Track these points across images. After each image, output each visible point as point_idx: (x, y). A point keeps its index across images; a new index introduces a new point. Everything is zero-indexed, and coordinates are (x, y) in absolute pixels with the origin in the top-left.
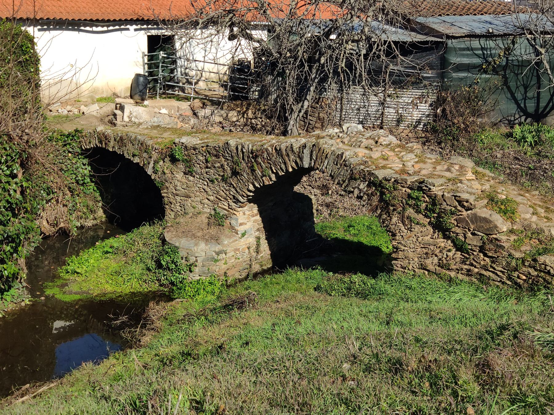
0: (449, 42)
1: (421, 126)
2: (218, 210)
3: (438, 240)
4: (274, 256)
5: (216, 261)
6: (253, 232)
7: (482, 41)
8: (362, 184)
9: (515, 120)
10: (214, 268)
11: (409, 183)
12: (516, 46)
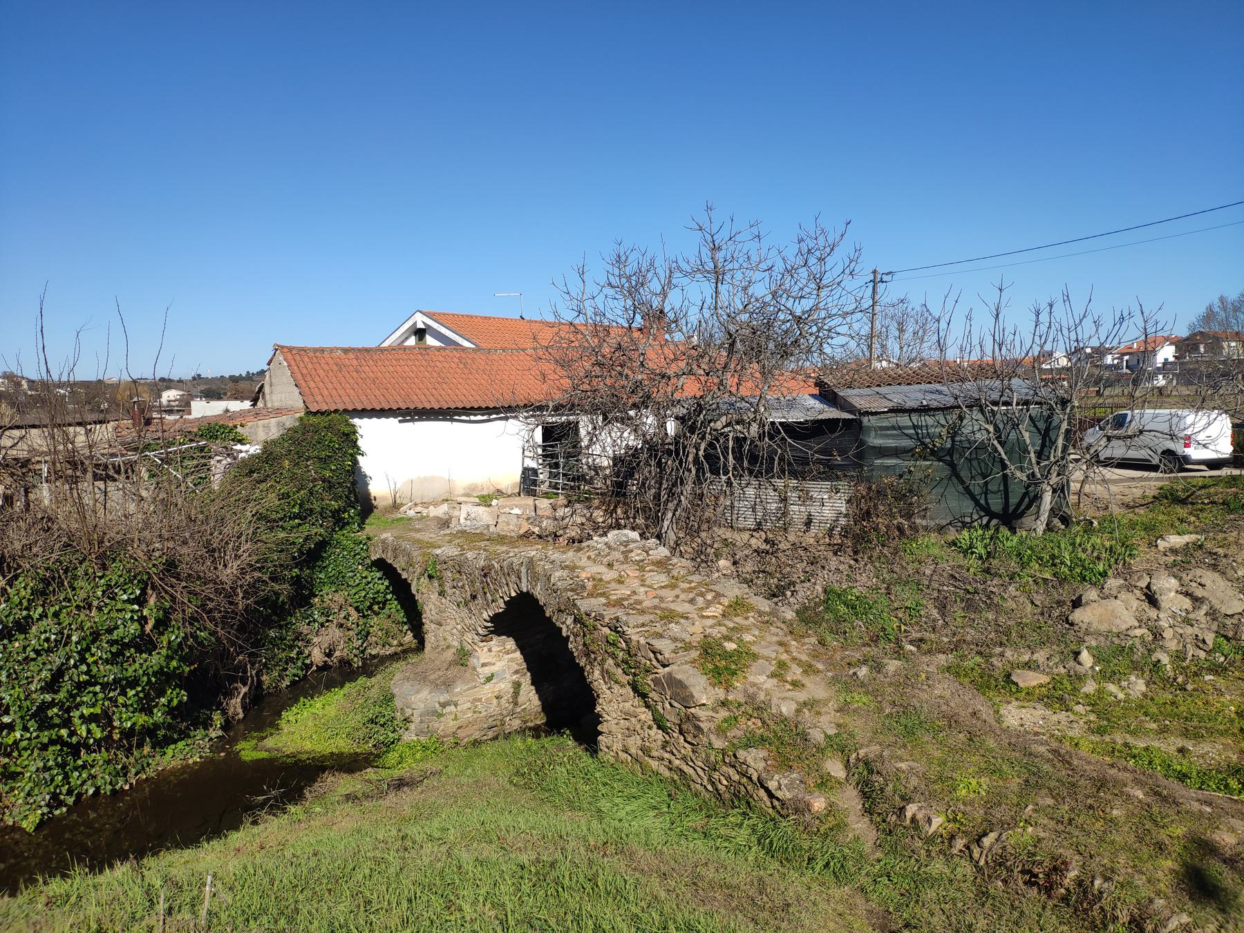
0: (865, 420)
2: (465, 644)
3: (638, 710)
4: (546, 707)
5: (441, 715)
6: (508, 676)
7: (915, 417)
10: (436, 725)
11: (607, 620)
12: (965, 422)
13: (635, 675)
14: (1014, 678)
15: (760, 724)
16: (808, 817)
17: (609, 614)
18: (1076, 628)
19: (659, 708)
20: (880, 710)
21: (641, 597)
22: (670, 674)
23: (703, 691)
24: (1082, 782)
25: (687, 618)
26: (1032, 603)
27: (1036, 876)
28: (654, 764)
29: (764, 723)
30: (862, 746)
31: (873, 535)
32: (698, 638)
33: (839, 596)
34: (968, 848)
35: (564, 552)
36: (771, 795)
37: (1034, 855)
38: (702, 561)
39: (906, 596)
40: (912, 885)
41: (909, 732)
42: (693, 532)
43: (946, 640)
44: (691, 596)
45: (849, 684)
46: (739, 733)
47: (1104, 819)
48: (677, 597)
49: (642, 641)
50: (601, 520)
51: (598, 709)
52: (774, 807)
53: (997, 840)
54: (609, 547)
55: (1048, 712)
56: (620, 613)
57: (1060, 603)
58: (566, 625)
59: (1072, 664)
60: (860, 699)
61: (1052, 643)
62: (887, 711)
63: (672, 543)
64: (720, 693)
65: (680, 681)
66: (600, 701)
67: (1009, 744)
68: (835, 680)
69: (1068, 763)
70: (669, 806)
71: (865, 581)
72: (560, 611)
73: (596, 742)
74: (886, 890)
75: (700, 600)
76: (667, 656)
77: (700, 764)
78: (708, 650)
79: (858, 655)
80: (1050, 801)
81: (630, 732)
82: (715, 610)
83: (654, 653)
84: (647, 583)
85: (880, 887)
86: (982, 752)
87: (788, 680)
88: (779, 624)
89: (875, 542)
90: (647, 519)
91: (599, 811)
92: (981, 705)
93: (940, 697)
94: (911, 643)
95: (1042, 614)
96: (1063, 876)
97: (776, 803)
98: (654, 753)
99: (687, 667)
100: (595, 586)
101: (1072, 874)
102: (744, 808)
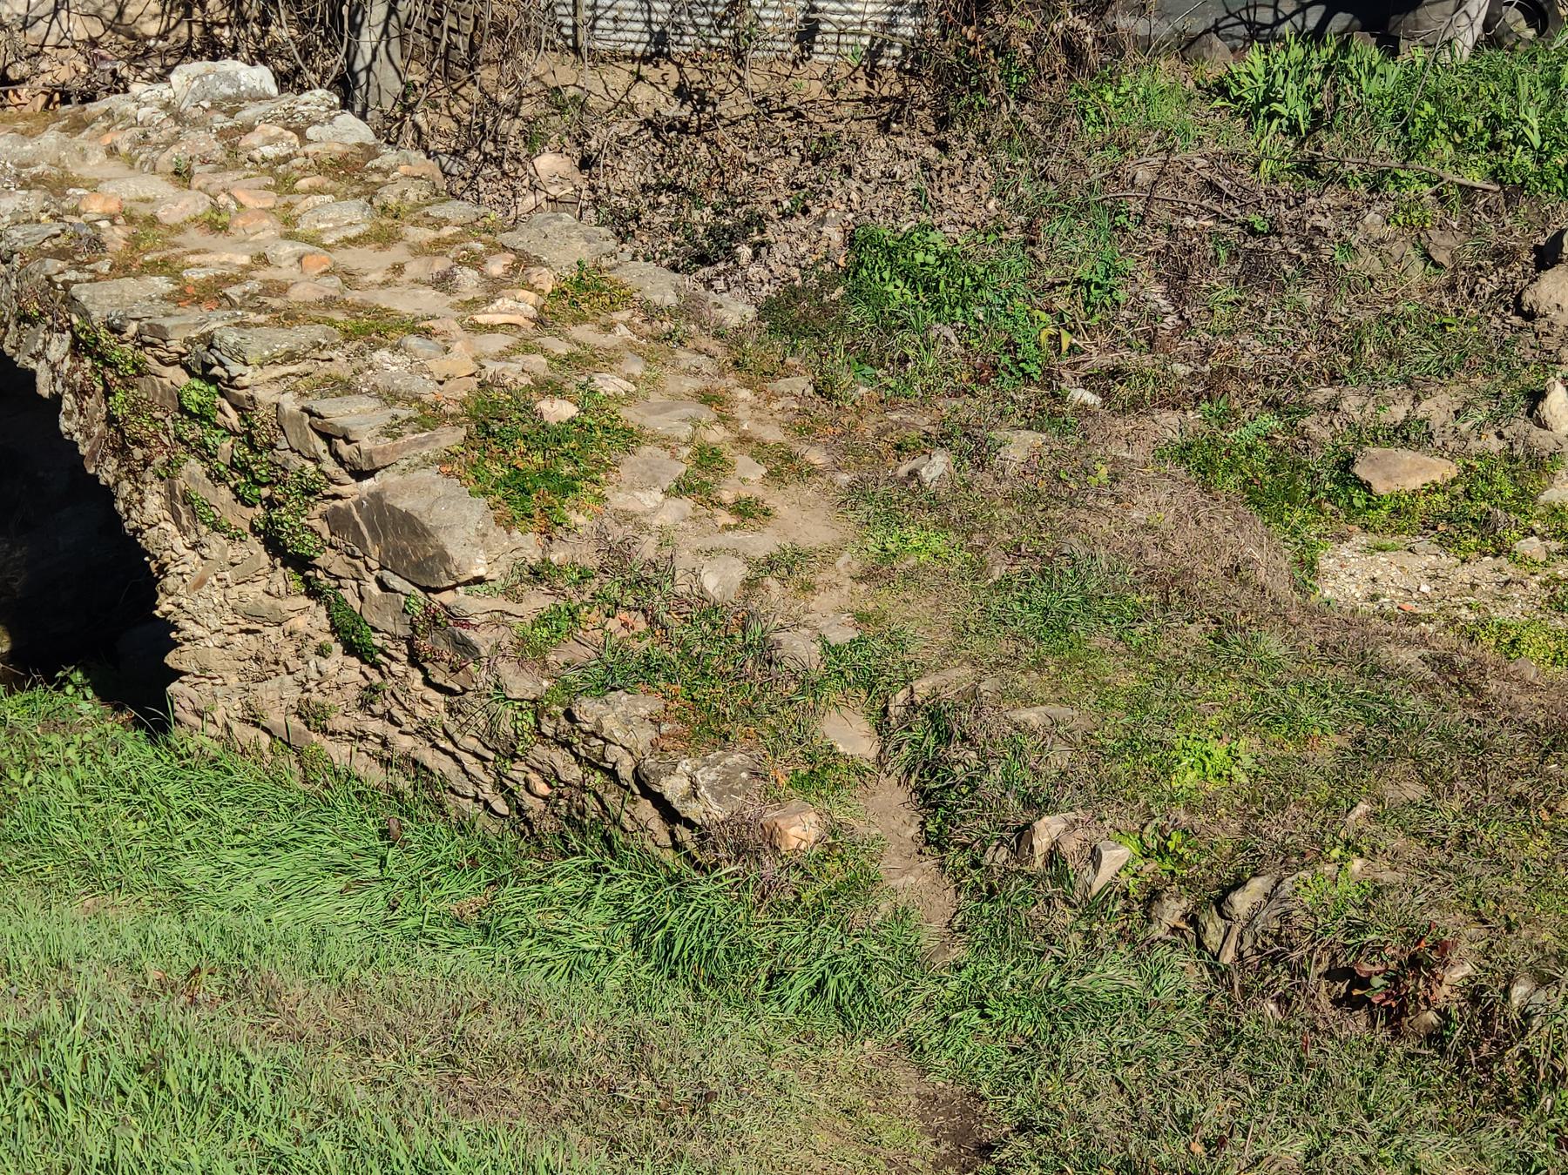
1: (897, 52)
3: (286, 604)
8: (55, 342)
9: (1278, 22)
11: (176, 345)
13: (271, 503)
14: (1360, 470)
15: (641, 625)
16: (770, 867)
17: (183, 327)
18: (1541, 325)
19: (349, 595)
20: (978, 570)
21: (285, 271)
22: (376, 497)
23: (476, 540)
24: (1505, 738)
25: (427, 333)
26: (1427, 257)
27: (1364, 983)
28: (338, 752)
29: (653, 621)
30: (924, 670)
31: (993, 73)
32: (462, 389)
33: (890, 253)
34: (1193, 921)
35: (27, 134)
36: (670, 814)
37: (1362, 929)
38: (487, 158)
39: (1077, 247)
40: (1044, 1025)
41: (1056, 626)
42: (453, 66)
43: (1181, 369)
44: (441, 265)
45: (884, 500)
46: (581, 654)
47: (1553, 830)
48: (398, 269)
49: (290, 404)
50: (152, 28)
51: (165, 605)
52: (677, 846)
53: (1269, 897)
54: (178, 117)
55: (1448, 561)
56: (217, 323)
57: (1503, 256)
58: (49, 361)
59: (1521, 425)
60: (923, 543)
61: (1472, 371)
62: (997, 573)
63: (388, 103)
64: (529, 545)
65: (407, 518)
66: (170, 582)
67: (1322, 647)
68: (857, 493)
69: (1474, 689)
70: (383, 862)
71: (964, 208)
72: (24, 318)
73: (162, 701)
74: (977, 1044)
75: (468, 279)
76: (366, 445)
77: (472, 743)
78: (491, 422)
79: (924, 422)
80: (1415, 791)
81: (265, 667)
82: (515, 307)
83: (327, 437)
84: (303, 227)
85: (956, 1036)
86: (1246, 670)
87: (728, 502)
88: (705, 342)
89: (999, 88)
90: (305, 24)
91: (178, 887)
92: (1264, 552)
93: (1148, 528)
94: (1087, 382)
95: (1452, 288)
96: (1433, 980)
97: (684, 834)
98: (338, 723)
99: (430, 474)
100: (134, 242)
101: (1459, 973)
102: (595, 852)
